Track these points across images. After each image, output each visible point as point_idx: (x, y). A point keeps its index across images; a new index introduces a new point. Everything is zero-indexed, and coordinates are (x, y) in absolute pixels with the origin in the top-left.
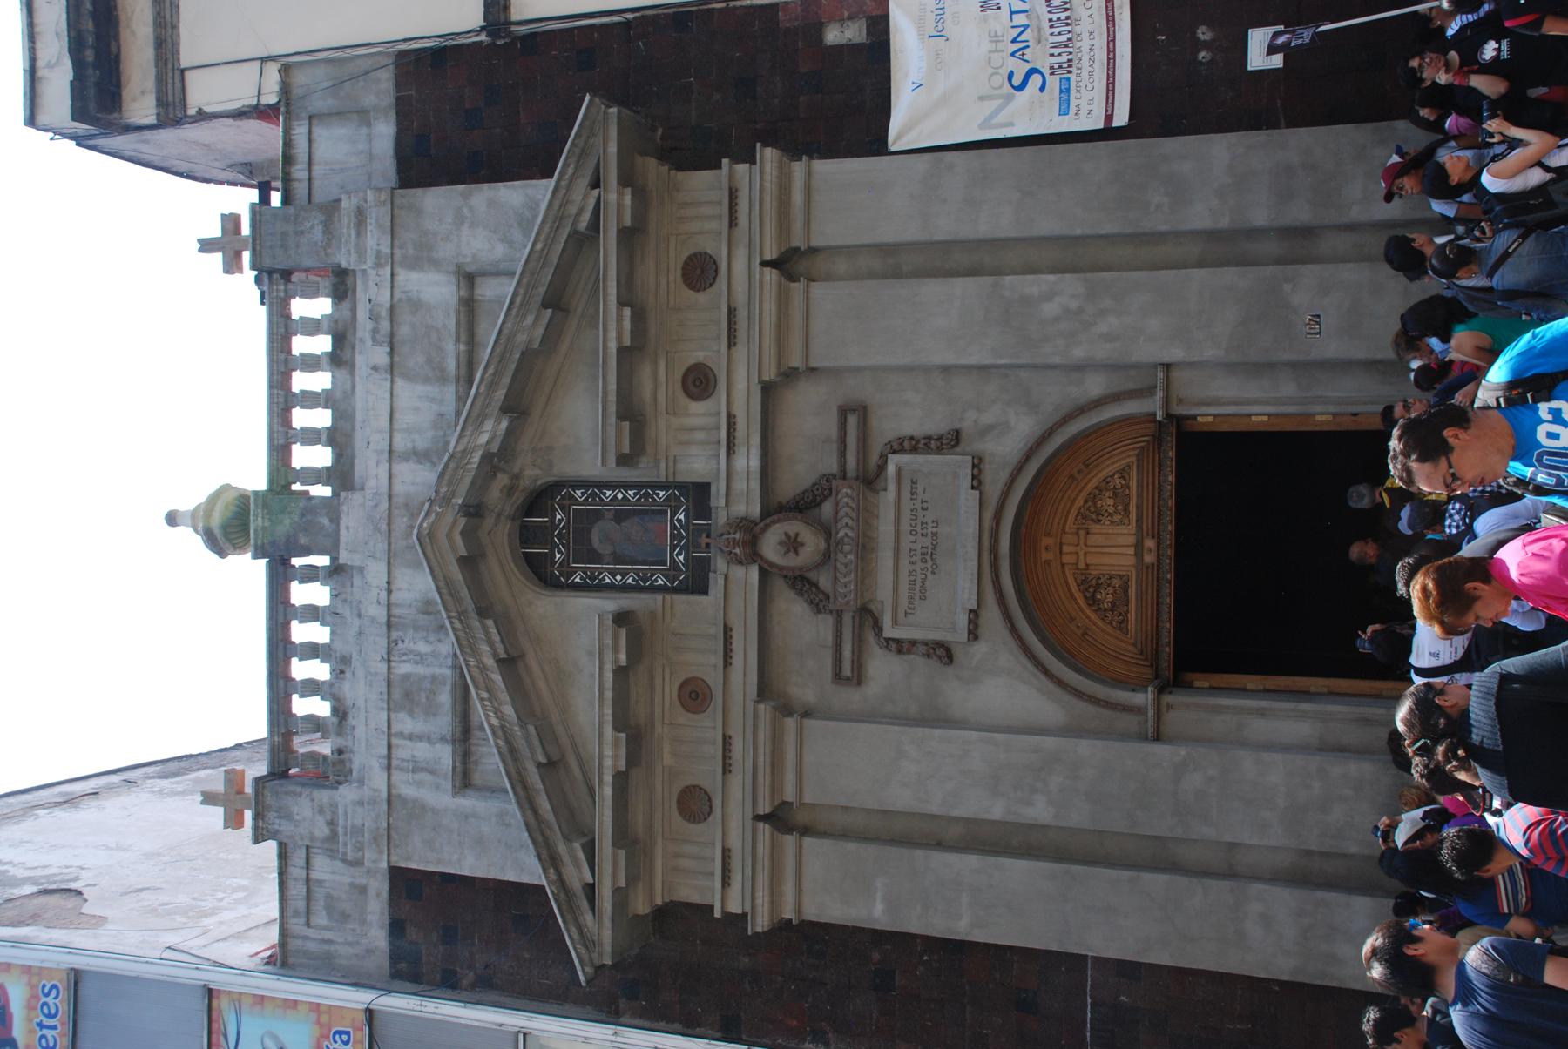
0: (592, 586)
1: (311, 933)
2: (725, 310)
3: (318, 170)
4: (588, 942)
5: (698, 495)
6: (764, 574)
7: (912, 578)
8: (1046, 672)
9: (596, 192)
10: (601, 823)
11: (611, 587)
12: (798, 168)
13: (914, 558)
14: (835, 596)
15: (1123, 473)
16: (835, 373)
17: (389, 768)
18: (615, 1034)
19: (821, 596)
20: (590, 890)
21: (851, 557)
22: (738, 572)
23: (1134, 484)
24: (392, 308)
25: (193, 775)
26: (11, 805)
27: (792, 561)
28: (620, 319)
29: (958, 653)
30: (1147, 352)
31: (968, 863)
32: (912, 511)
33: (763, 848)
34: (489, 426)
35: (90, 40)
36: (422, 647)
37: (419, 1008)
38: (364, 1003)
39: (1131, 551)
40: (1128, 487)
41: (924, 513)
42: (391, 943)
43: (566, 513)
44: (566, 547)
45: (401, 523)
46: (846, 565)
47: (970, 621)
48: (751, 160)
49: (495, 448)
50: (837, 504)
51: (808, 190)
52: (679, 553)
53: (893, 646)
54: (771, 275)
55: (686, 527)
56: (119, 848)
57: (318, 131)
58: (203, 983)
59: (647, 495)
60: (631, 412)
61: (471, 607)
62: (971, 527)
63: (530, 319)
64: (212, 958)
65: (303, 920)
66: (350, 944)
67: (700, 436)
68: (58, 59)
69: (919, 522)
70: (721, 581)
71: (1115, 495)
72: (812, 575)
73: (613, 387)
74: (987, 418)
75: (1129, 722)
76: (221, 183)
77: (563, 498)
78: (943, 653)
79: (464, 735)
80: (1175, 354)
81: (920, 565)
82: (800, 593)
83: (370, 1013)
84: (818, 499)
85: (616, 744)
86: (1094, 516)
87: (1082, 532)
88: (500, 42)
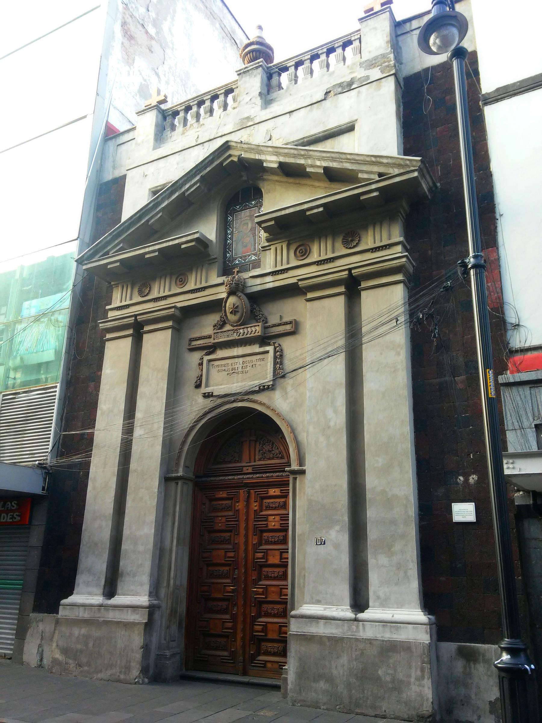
29: (198, 390)
33: (507, 380)
52: (239, 261)
69: (248, 364)
81: (230, 367)
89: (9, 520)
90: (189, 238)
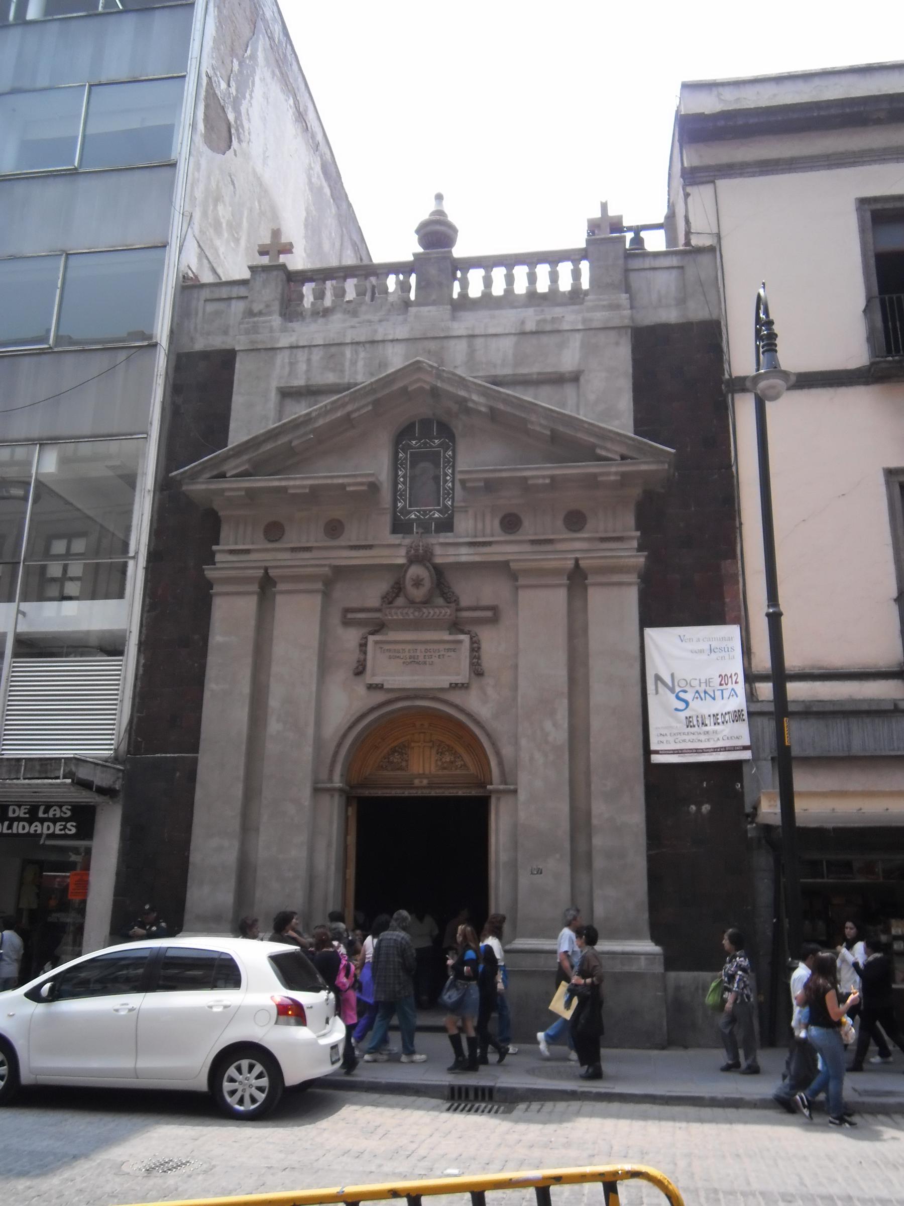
0: (396, 464)
1: (202, 302)
2: (551, 537)
3: (650, 274)
4: (193, 476)
5: (446, 526)
6: (401, 566)
7: (401, 651)
8: (350, 728)
9: (618, 458)
10: (259, 480)
11: (396, 476)
12: (633, 578)
13: (412, 652)
14: (390, 608)
15: (465, 766)
16: (515, 603)
17: (292, 347)
18: (149, 491)
19: (390, 599)
20: (222, 476)
21: (411, 617)
22: (403, 552)
23: (458, 772)
24: (559, 331)
25: (325, 184)
26: (296, 80)
27: (408, 583)
28: (544, 477)
30: (523, 779)
31: (245, 688)
32: (439, 649)
34: (482, 400)
35: (731, 123)
36: (360, 364)
37: (159, 374)
38: (161, 341)
39: (421, 772)
40: (456, 769)
41: (437, 656)
42: (197, 352)
43: (438, 446)
44: (419, 447)
45: (433, 346)
46: (407, 613)
47: (377, 685)
48: (640, 549)
49: (471, 405)
50: (441, 607)
51: (620, 584)
53: (363, 642)
54: (570, 564)
55: (431, 518)
56: (265, 158)
57: (674, 273)
58: (170, 242)
59: (449, 494)
60: (491, 486)
61: (379, 395)
62: (429, 685)
63: (543, 422)
64: (185, 244)
65: (208, 297)
66: (195, 328)
67: (480, 526)
68: (723, 100)
70: (397, 542)
71: (452, 762)
72: (402, 594)
73: (504, 475)
74: (490, 691)
75: (324, 775)
76: (669, 195)
77: (448, 444)
78: (360, 671)
79: (310, 392)
80: (522, 796)
81: (407, 654)
82: (393, 587)
83: (155, 345)
84: (445, 595)
85: (303, 487)
86: (440, 750)
87: (431, 744)
88: (723, 387)
89: (57, 832)
90: (359, 480)
